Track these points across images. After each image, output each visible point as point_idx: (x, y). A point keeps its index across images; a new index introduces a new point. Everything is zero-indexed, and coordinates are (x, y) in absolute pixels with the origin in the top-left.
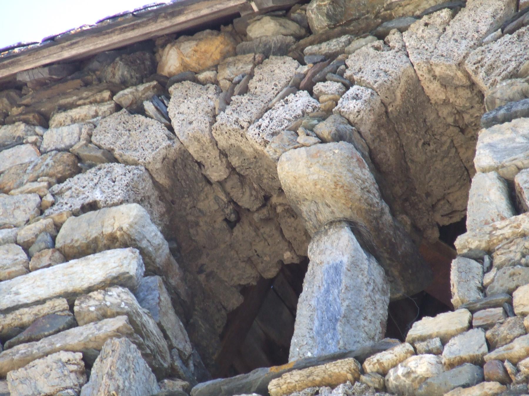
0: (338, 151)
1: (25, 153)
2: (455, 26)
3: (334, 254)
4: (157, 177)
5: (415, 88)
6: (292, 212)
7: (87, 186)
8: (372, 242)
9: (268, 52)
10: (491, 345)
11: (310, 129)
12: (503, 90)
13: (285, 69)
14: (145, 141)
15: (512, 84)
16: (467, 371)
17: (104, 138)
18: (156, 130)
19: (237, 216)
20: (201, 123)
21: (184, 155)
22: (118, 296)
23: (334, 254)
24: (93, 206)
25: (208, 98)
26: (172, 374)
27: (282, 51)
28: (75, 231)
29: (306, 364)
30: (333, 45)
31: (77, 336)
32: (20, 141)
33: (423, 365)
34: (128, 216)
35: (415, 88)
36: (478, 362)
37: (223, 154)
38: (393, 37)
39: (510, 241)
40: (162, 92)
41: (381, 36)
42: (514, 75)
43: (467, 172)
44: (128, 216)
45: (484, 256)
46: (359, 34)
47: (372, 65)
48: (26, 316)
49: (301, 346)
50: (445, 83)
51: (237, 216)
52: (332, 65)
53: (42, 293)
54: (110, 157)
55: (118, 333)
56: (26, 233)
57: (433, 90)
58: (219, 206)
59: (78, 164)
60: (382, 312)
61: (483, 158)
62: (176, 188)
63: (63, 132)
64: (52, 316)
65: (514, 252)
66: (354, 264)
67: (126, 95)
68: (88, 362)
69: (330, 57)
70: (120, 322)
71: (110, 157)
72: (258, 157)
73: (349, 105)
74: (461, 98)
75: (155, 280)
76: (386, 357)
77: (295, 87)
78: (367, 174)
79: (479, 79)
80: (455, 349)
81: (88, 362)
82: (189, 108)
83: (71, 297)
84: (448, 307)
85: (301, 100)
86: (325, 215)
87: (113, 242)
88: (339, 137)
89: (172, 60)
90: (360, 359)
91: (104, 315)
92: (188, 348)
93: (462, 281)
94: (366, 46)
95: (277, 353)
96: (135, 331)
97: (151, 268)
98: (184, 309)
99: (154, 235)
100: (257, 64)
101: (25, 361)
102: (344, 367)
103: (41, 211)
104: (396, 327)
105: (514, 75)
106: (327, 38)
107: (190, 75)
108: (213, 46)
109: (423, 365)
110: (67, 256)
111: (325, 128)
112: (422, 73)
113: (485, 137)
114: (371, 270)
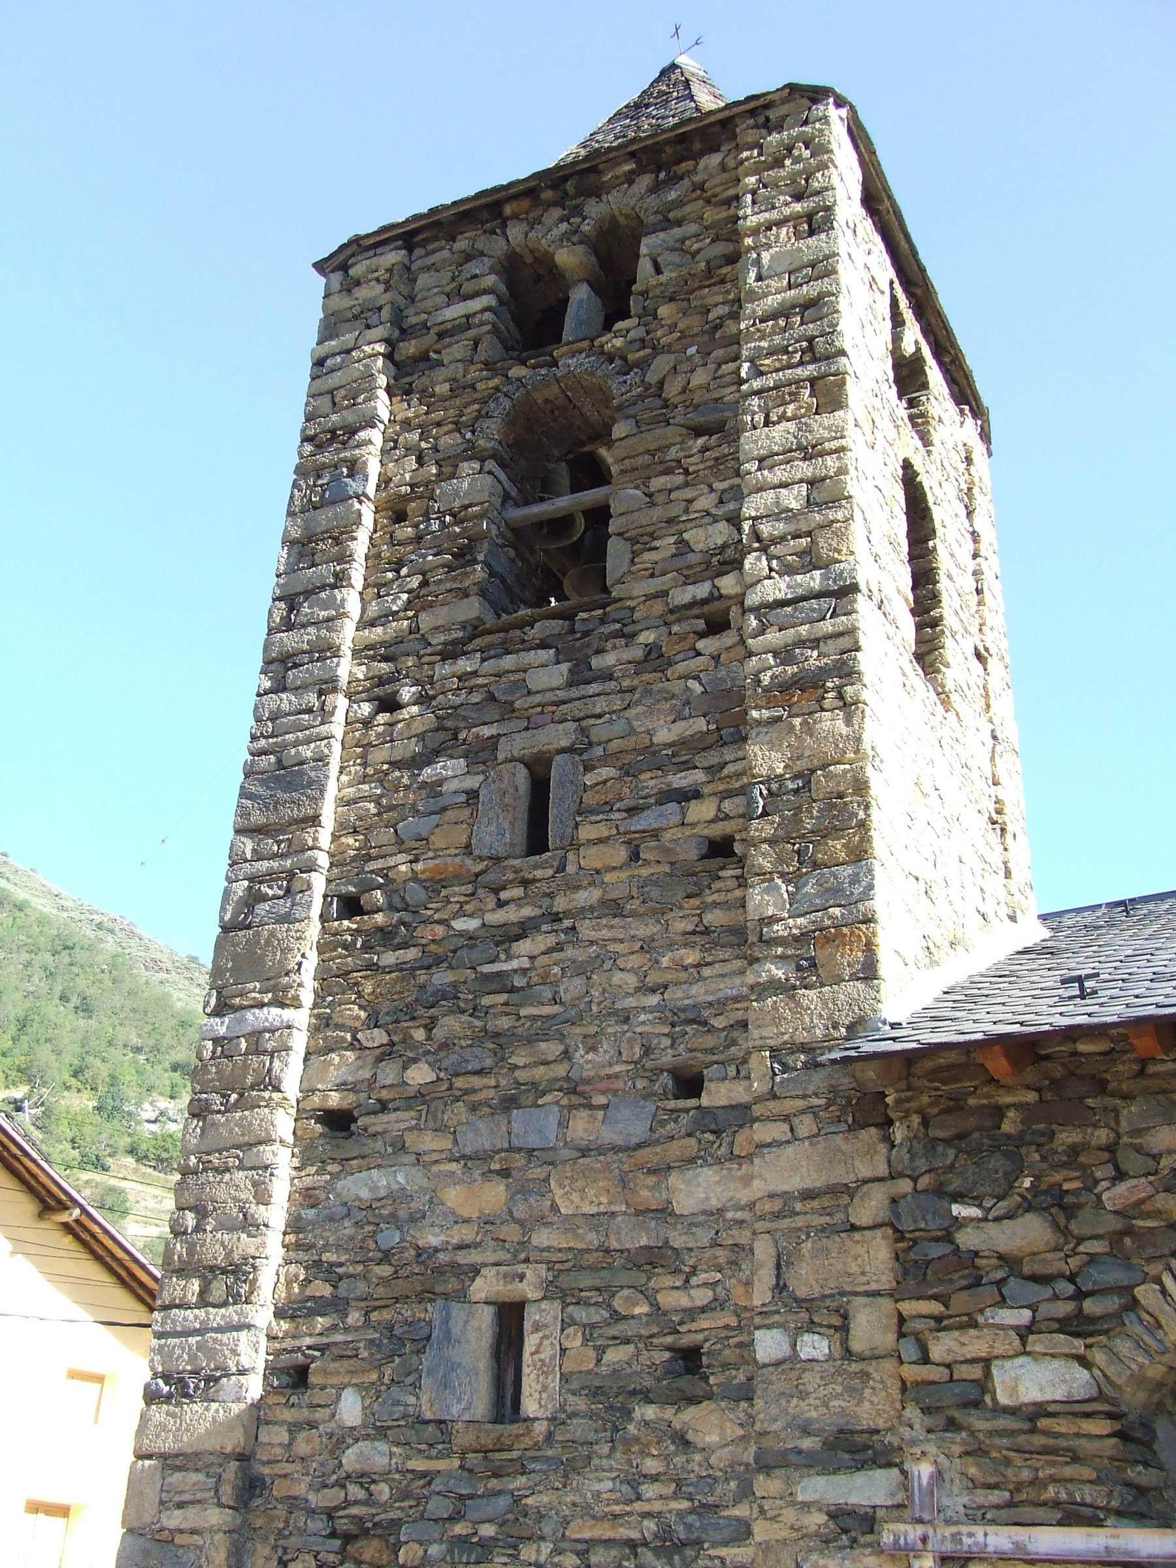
0: (580, 249)
1: (445, 254)
2: (630, 191)
3: (581, 294)
4: (606, 1052)
5: (613, 218)
6: (562, 276)
7: (474, 268)
8: (596, 288)
9: (550, 205)
10: (648, 333)
11: (569, 240)
12: (652, 219)
13: (557, 212)
14: (497, 246)
15: (949, 577)
16: (638, 345)
17: (480, 246)
18: (502, 242)
19: (538, 279)
20: (521, 237)
21: (514, 253)
22: (487, 316)
23: (581, 294)
24: (476, 276)
25: (524, 227)
26: (513, 349)
27: (555, 204)
28: (468, 287)
29: (569, 343)
30: (578, 201)
31: (471, 333)
32: (443, 248)
33: (618, 342)
34: (491, 280)
35: (613, 218)
36: (643, 340)
37: (531, 251)
38: (604, 197)
39: (655, 286)
40: (504, 225)
41: (599, 196)
42: (656, 213)
43: (637, 256)
44: (491, 280)
45: (645, 294)
46: (589, 196)
47: (595, 209)
48: (449, 326)
49: (567, 335)
50: (627, 216)
51: (538, 279)
52: (577, 211)
53: (455, 315)
54: (482, 254)
55: (489, 332)
56: (447, 289)
57: (622, 220)
58: (765, 1366)
59: (468, 257)
60: (602, 319)
61: (643, 250)
62: (512, 267)
63: (462, 244)
64: (459, 325)
65: (657, 292)
66: (589, 298)
67: (488, 226)
68: (476, 344)
69: (577, 206)
70: (489, 327)
71: (482, 254)
72: (547, 252)
73: (585, 228)
74: (634, 224)
75: (504, 308)
76: (604, 339)
77: (561, 220)
78: (594, 259)
79: (642, 214)
80: (632, 335)
81: (476, 344)
82: (515, 232)
83: (468, 317)
84: (629, 316)
85: (564, 227)
86: (576, 277)
87: (485, 292)
88: (581, 242)
89: (508, 210)
90: (592, 341)
91: (482, 324)
92: (518, 337)
93: (634, 305)
94: (592, 201)
95: (557, 339)
96: (495, 331)
97: (501, 302)
98: (516, 320)
99: (502, 288)
100: (545, 210)
101: (449, 345)
102: (585, 344)
103: (453, 279)
104: (607, 327)
105: (656, 213)
106: (575, 197)
107: (515, 216)
108: (525, 203)
109: (618, 342)
110: (466, 298)
111: (575, 239)
112: (617, 213)
113: (644, 241)
114: (597, 301)
